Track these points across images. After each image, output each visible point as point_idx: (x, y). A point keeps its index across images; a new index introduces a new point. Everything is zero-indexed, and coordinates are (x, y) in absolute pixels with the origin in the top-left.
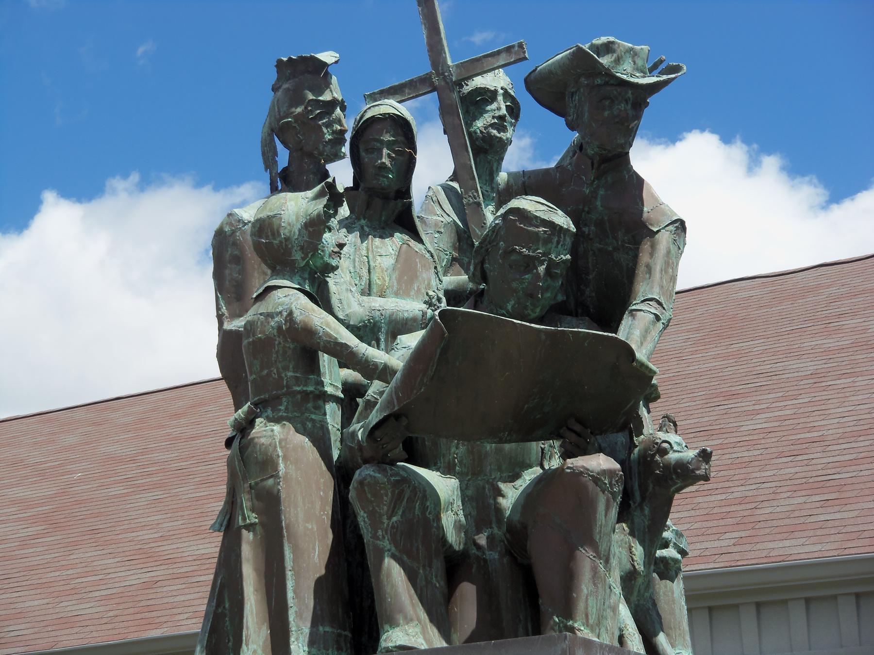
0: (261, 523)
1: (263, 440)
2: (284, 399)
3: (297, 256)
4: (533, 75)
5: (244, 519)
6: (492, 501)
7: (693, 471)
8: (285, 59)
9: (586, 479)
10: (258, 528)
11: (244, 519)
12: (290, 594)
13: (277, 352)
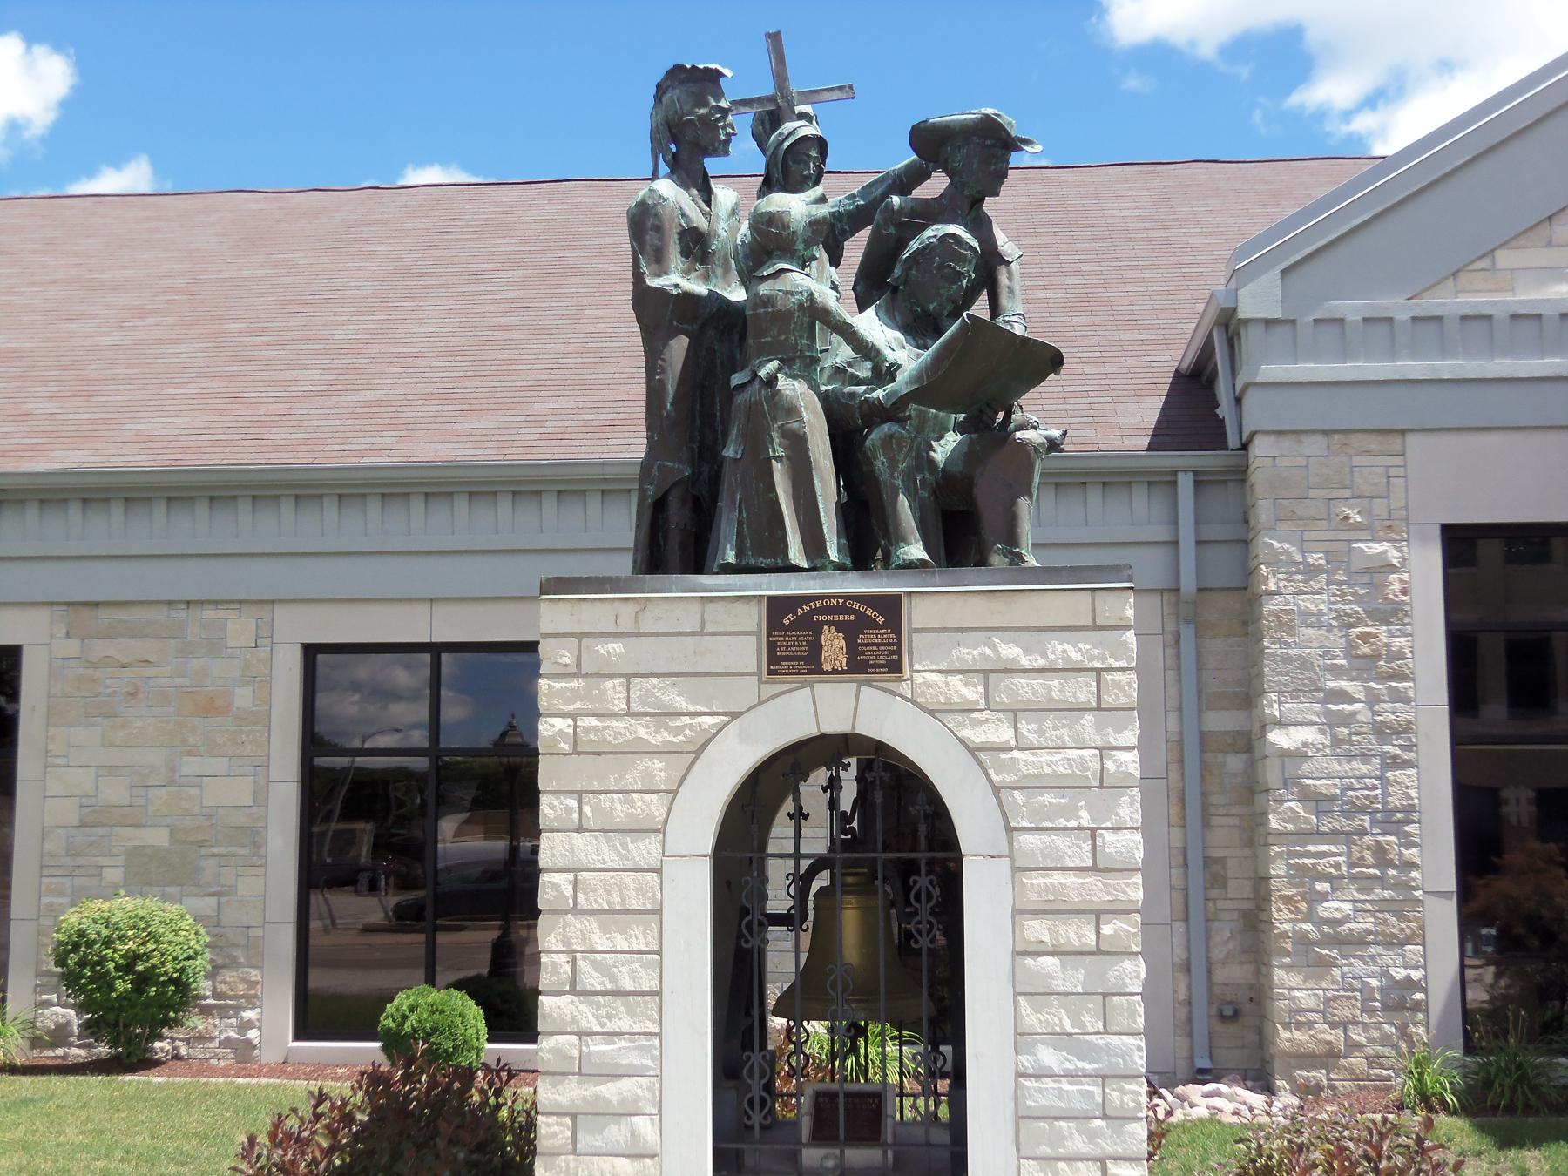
0: (787, 456)
1: (788, 392)
2: (797, 361)
3: (800, 246)
4: (922, 125)
5: (774, 452)
6: (924, 454)
7: (1059, 445)
8: (688, 66)
9: (1030, 448)
10: (784, 459)
11: (774, 452)
12: (822, 514)
13: (796, 323)
